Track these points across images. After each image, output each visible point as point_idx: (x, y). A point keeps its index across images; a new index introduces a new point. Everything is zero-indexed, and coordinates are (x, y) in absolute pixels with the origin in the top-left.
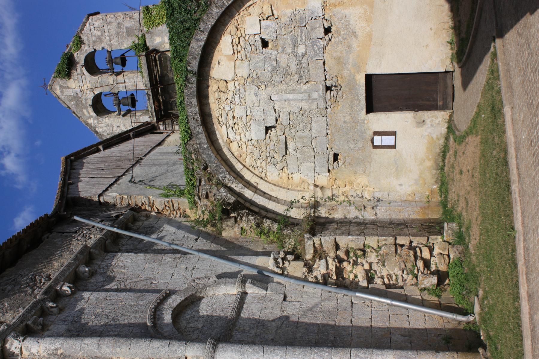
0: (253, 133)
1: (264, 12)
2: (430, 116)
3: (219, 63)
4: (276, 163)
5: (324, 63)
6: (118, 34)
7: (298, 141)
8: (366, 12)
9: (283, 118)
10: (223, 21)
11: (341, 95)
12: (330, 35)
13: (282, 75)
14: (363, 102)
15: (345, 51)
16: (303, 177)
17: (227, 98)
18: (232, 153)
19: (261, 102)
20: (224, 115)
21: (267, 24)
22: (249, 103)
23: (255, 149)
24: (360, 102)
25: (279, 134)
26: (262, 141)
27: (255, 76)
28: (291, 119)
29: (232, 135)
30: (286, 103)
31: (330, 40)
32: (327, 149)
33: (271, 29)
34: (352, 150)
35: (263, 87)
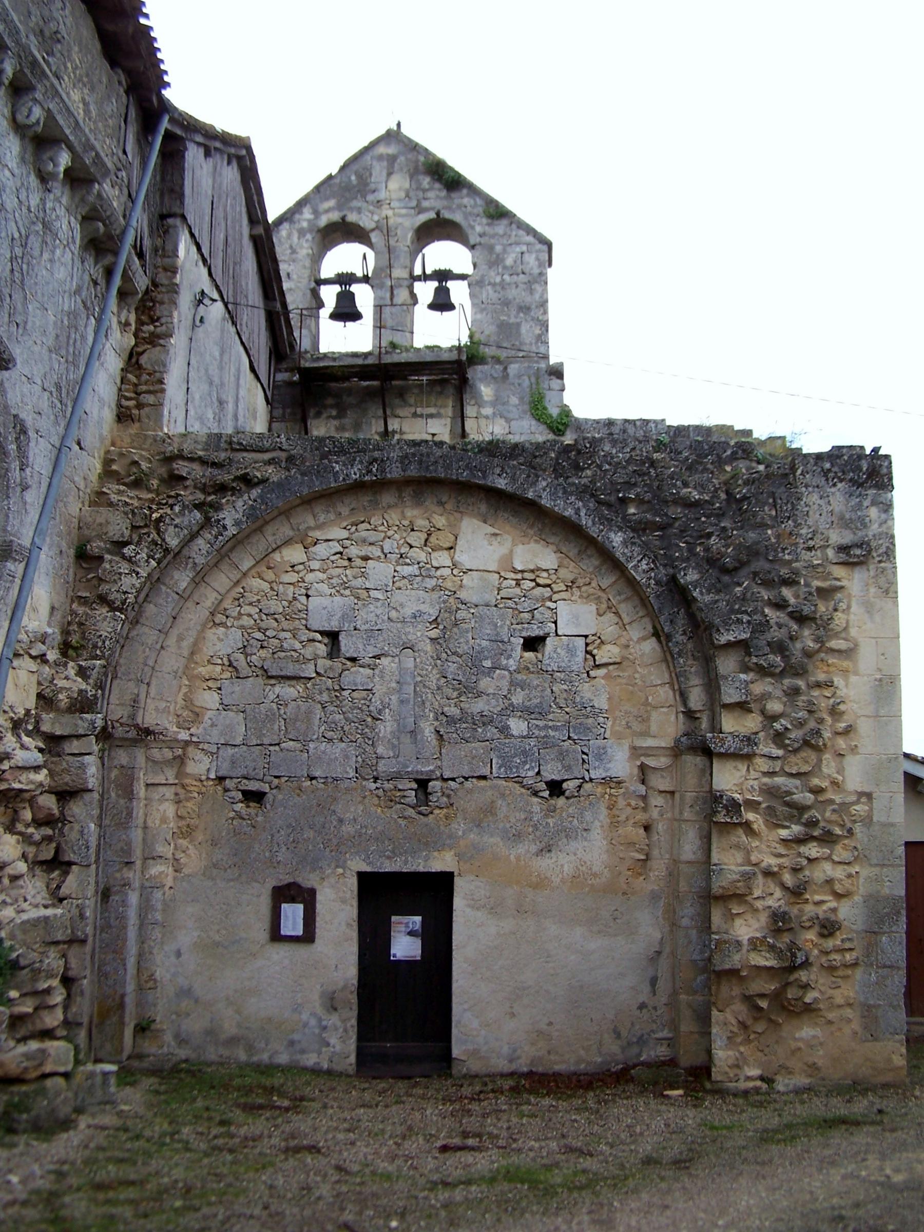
0: (326, 601)
1: (604, 647)
2: (349, 1025)
3: (495, 535)
4: (249, 650)
5: (484, 778)
6: (506, 303)
7: (298, 707)
8: (595, 875)
9: (358, 676)
10: (589, 553)
11: (406, 814)
12: (546, 794)
13: (460, 678)
14: (388, 867)
15: (508, 826)
16: (209, 714)
17: (411, 547)
18: (278, 547)
19: (399, 625)
20: (372, 536)
21: (578, 653)
22: (398, 597)
23: (285, 603)
24: (389, 858)
25: (321, 662)
26: (304, 622)
27: (461, 614)
28: (355, 694)
29: (321, 550)
30: (394, 685)
31: (535, 794)
32: (276, 777)
33: (566, 660)
34: (272, 836)
35: (434, 633)
